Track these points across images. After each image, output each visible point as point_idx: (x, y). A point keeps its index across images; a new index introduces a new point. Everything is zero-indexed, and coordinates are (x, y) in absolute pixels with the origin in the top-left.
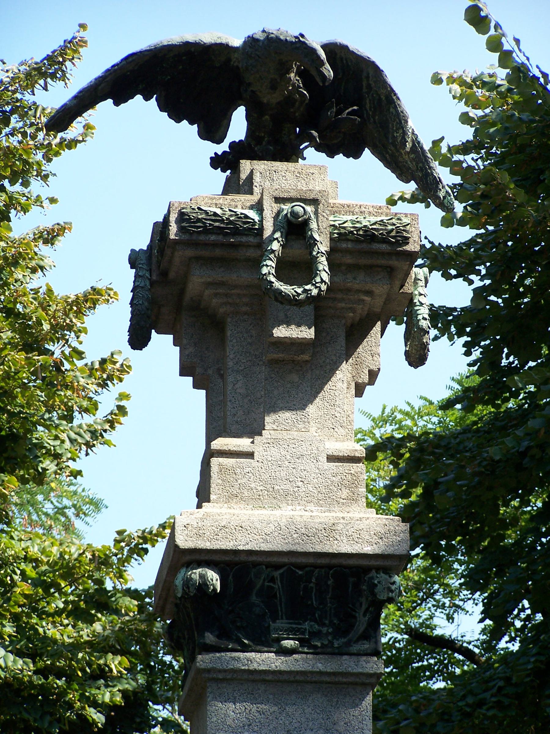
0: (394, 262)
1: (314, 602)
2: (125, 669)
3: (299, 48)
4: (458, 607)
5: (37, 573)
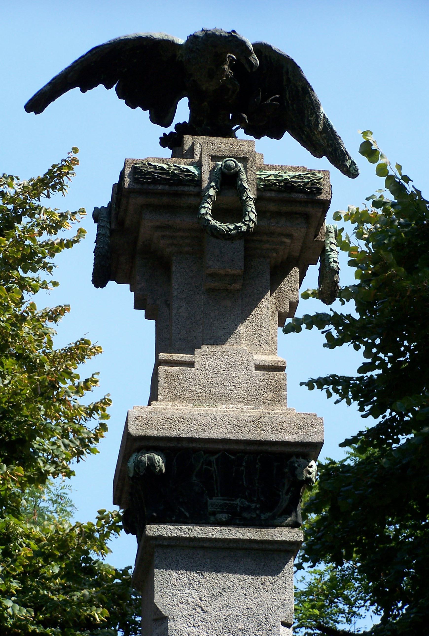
0: (310, 210)
1: (245, 483)
2: (106, 618)
3: (233, 41)
4: (354, 612)
5: (39, 547)
